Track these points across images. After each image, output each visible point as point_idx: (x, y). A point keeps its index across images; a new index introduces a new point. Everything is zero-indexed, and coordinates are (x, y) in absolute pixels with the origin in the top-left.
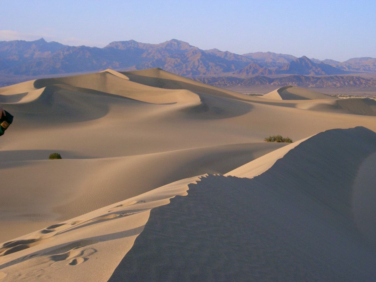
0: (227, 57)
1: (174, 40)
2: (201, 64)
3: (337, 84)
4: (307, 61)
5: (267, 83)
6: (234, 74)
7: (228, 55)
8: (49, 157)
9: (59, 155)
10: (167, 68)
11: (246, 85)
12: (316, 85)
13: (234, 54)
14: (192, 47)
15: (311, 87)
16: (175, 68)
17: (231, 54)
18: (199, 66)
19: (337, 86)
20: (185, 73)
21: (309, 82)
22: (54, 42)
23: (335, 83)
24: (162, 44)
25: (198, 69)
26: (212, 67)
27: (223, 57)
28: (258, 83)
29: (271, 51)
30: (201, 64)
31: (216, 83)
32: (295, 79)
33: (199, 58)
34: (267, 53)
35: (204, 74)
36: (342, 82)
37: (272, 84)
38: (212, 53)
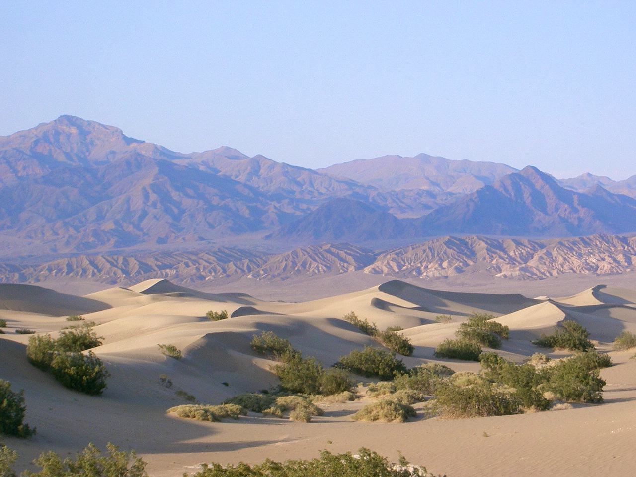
0: (259, 177)
1: (70, 120)
2: (154, 205)
3: (601, 264)
4: (539, 184)
5: (352, 269)
6: (268, 237)
7: (262, 172)
8: (289, 458)
9: (247, 465)
11: (274, 276)
12: (521, 269)
13: (285, 165)
14: (133, 145)
15: (505, 276)
16: (59, 224)
17: (274, 164)
18: (144, 214)
19: (599, 272)
20: (92, 239)
21: (501, 261)
23: (593, 260)
24: (23, 135)
25: (143, 224)
26: (192, 216)
27: (242, 178)
28: (318, 267)
29: (434, 152)
30: (154, 205)
31: (168, 271)
32: (450, 251)
33: (147, 182)
34: (416, 157)
35: (161, 241)
36: (620, 258)
37: (367, 270)
38: (204, 163)
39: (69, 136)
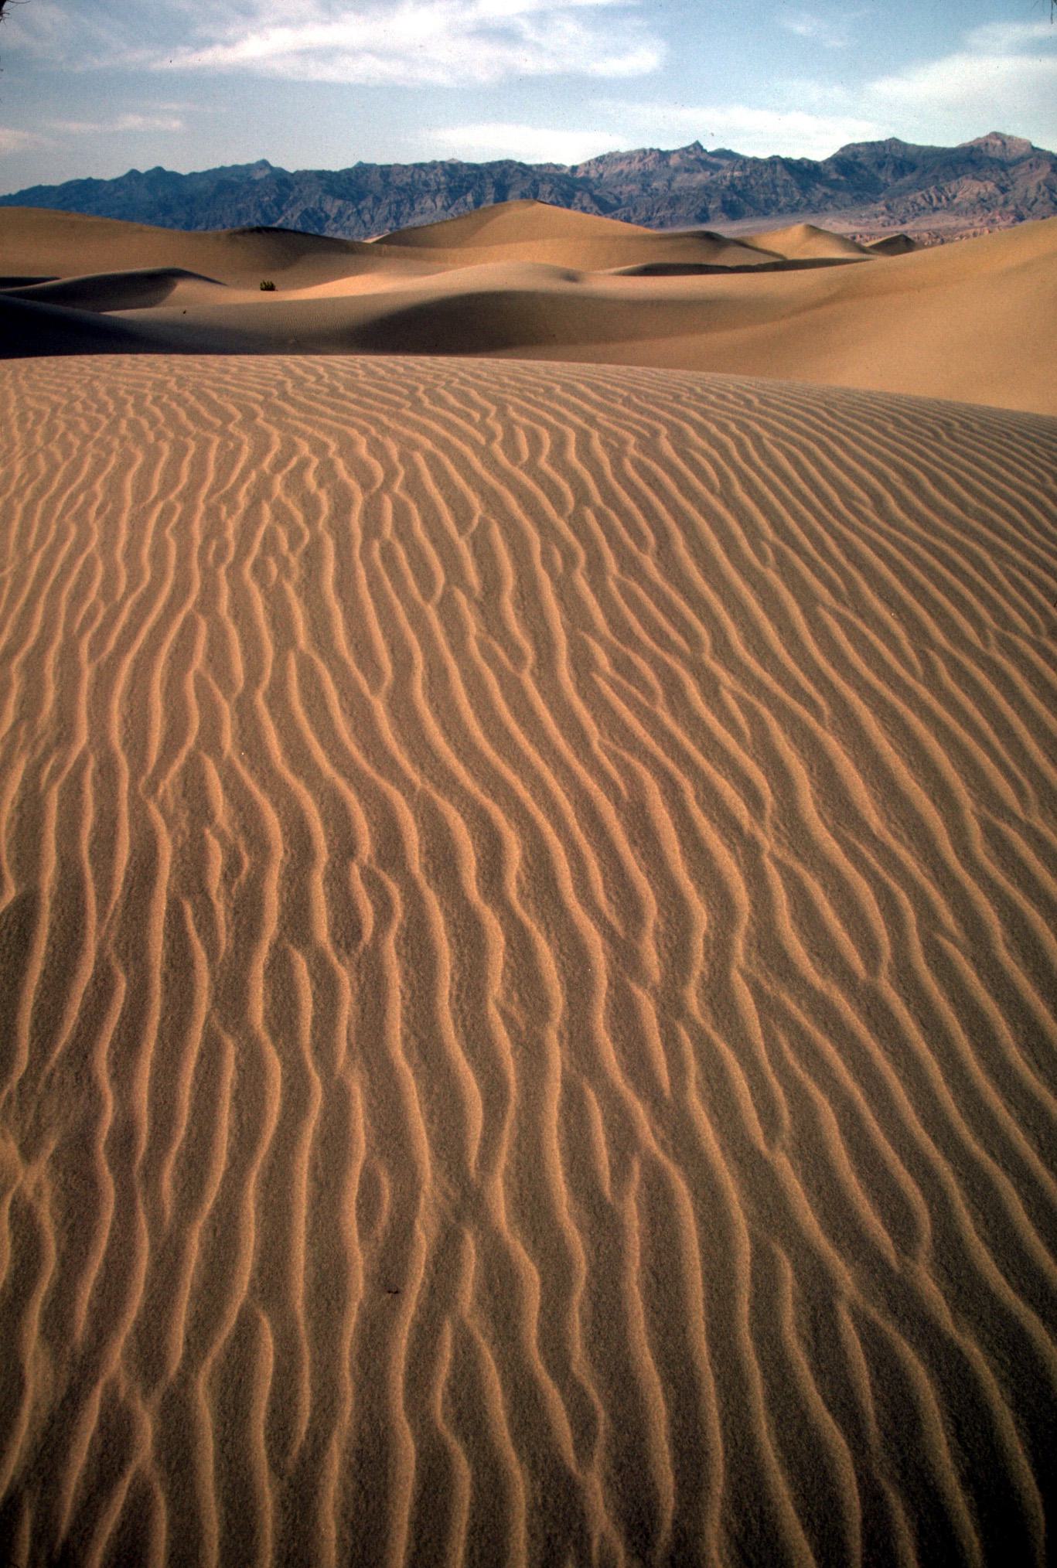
10: (958, 205)
22: (778, 157)
30: (1043, 194)
39: (995, 146)
